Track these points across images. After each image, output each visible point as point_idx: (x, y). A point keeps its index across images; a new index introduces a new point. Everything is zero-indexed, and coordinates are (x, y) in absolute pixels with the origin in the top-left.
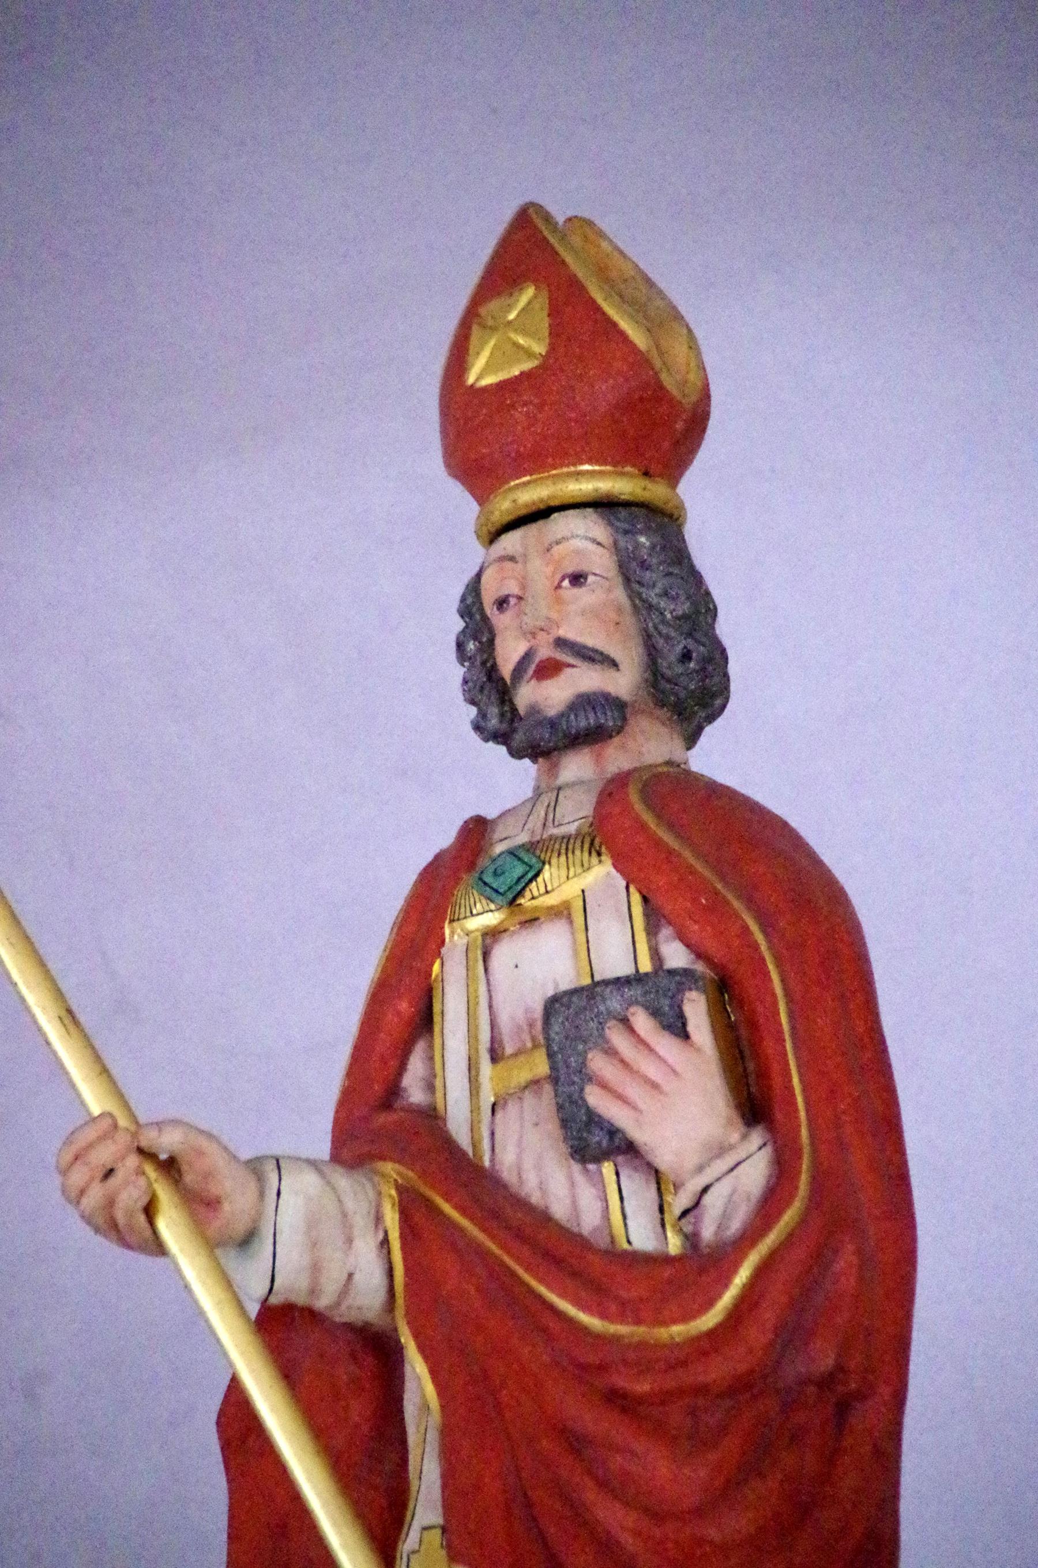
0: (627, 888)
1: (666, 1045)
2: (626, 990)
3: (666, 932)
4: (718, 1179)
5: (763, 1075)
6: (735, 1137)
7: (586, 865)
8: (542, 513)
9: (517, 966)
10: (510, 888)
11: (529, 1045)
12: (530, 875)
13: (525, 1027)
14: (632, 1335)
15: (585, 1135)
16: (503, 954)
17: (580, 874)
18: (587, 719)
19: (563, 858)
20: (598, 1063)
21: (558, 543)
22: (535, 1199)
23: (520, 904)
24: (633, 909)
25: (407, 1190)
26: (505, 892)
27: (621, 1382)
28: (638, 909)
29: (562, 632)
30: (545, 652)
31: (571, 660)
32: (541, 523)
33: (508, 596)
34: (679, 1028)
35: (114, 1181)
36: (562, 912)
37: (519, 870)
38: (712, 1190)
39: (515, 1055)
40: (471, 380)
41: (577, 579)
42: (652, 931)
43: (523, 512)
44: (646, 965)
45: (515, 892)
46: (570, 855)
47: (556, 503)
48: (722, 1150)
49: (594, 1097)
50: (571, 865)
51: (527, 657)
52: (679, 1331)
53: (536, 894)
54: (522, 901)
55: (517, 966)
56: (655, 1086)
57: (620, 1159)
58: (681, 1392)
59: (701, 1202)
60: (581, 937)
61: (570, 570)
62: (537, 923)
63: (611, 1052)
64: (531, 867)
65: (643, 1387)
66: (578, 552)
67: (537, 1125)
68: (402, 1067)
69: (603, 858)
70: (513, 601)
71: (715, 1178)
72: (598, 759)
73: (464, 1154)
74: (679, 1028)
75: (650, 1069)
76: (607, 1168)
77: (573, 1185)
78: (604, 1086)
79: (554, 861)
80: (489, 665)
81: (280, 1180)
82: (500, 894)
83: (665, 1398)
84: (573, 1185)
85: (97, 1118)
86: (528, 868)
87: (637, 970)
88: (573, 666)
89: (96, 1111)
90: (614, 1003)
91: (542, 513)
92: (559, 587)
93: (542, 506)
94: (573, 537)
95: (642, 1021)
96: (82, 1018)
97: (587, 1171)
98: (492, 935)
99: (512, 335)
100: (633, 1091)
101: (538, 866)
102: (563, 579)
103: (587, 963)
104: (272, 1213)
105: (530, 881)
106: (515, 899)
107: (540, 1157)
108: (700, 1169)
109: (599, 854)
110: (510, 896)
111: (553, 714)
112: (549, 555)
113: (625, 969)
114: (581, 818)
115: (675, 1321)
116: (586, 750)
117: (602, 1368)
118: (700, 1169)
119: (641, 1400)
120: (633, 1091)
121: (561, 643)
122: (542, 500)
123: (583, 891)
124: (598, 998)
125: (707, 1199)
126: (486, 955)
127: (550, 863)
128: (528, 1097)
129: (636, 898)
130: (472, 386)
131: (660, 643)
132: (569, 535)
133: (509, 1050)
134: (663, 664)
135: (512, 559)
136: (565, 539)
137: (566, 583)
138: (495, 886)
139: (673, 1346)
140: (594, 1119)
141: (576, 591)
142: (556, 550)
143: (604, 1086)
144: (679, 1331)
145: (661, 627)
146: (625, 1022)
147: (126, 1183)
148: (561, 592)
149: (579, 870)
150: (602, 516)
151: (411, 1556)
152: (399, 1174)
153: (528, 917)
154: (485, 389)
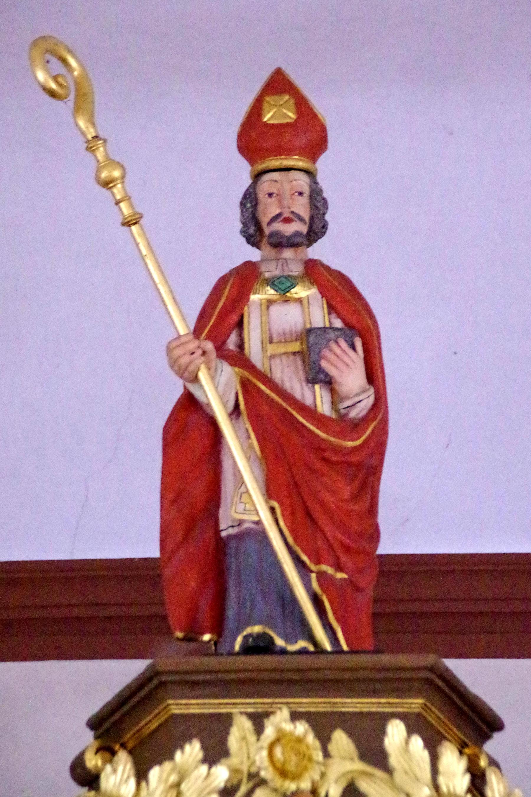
1: (350, 352)
3: (333, 315)
11: (283, 340)
16: (275, 310)
20: (326, 352)
21: (295, 180)
22: (289, 390)
28: (325, 306)
30: (287, 214)
32: (287, 172)
35: (193, 356)
36: (300, 301)
37: (289, 284)
38: (362, 402)
39: (276, 343)
40: (265, 120)
41: (301, 194)
42: (329, 313)
47: (294, 167)
48: (364, 391)
49: (324, 364)
51: (279, 215)
52: (350, 444)
56: (347, 365)
61: (300, 190)
63: (331, 350)
65: (335, 459)
68: (228, 336)
70: (275, 195)
74: (353, 347)
75: (346, 359)
76: (317, 387)
78: (328, 360)
85: (182, 336)
92: (293, 194)
93: (289, 167)
95: (344, 344)
98: (270, 303)
99: (285, 111)
100: (341, 365)
108: (357, 395)
116: (293, 249)
118: (357, 395)
121: (293, 213)
126: (268, 307)
128: (284, 358)
129: (325, 302)
133: (275, 340)
134: (314, 227)
137: (296, 194)
140: (321, 370)
142: (294, 183)
143: (328, 360)
146: (337, 343)
148: (293, 197)
153: (287, 299)
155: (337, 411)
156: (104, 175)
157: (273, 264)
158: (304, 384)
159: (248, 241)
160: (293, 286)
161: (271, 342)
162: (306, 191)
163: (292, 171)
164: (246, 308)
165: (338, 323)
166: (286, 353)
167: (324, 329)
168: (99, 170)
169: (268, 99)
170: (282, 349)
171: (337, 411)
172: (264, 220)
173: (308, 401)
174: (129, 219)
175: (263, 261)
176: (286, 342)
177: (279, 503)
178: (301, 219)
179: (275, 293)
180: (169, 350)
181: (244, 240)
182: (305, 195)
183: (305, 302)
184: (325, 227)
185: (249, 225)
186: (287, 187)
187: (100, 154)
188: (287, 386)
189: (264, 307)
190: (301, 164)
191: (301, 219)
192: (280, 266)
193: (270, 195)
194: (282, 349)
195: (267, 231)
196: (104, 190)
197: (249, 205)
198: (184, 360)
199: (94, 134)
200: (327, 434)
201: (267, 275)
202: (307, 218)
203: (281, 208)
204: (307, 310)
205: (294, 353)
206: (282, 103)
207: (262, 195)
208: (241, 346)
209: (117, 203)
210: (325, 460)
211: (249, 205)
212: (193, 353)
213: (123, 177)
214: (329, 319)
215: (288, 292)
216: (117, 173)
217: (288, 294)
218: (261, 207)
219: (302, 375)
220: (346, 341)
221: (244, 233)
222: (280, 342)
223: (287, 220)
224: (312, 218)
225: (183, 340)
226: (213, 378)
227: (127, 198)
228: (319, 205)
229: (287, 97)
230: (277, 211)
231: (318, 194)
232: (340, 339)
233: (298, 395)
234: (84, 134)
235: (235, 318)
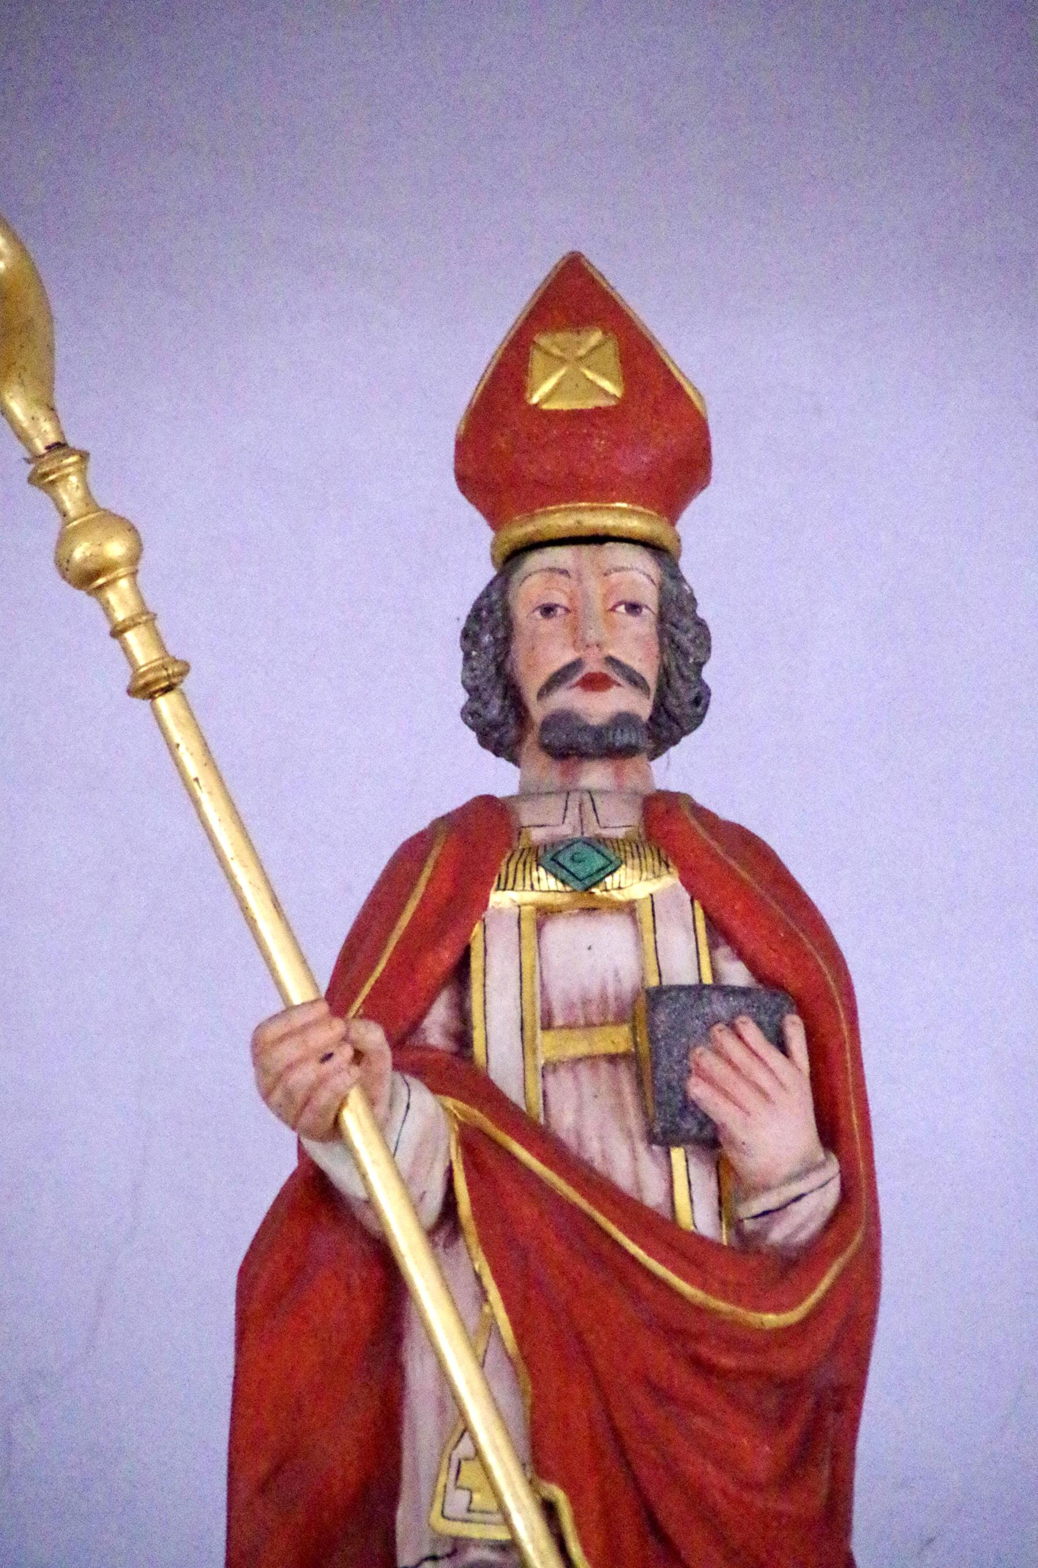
0: (692, 901)
1: (774, 1057)
2: (731, 999)
3: (724, 951)
4: (811, 1191)
5: (834, 1104)
6: (821, 1156)
7: (657, 873)
8: (599, 539)
9: (590, 948)
10: (591, 875)
11: (582, 1022)
12: (609, 869)
13: (579, 1005)
14: (732, 1313)
15: (678, 1119)
16: (557, 932)
17: (651, 879)
18: (631, 736)
19: (637, 861)
21: (617, 570)
23: (593, 893)
24: (698, 924)
25: (465, 1125)
26: (584, 879)
27: (704, 1350)
28: (701, 924)
29: (612, 652)
30: (593, 666)
31: (619, 679)
32: (594, 547)
33: (557, 606)
34: (782, 1046)
35: (328, 1066)
36: (629, 909)
37: (600, 862)
38: (805, 1199)
39: (562, 1027)
41: (634, 608)
42: (713, 946)
43: (583, 533)
44: (708, 979)
45: (594, 881)
46: (642, 859)
49: (698, 1090)
50: (644, 869)
52: (772, 1320)
53: (609, 887)
54: (594, 890)
55: (590, 948)
57: (690, 1147)
58: (757, 1374)
59: (789, 1207)
60: (648, 937)
61: (629, 598)
62: (597, 912)
63: (718, 1052)
64: (611, 862)
65: (727, 1361)
66: (633, 582)
67: (596, 1096)
68: (423, 1015)
69: (671, 870)
71: (809, 1190)
72: (618, 774)
73: (516, 1106)
74: (782, 1046)
76: (677, 1155)
77: (635, 1159)
78: (709, 1080)
79: (630, 862)
80: (499, 659)
81: (409, 1095)
82: (577, 878)
83: (741, 1375)
84: (635, 1159)
86: (608, 863)
87: (701, 980)
88: (619, 685)
89: (297, 999)
90: (720, 1007)
91: (599, 539)
94: (633, 569)
95: (751, 1032)
96: (285, 908)
97: (652, 1150)
98: (545, 914)
100: (743, 1091)
101: (617, 863)
102: (620, 603)
103: (655, 962)
104: (399, 1124)
105: (608, 875)
106: (590, 887)
107: (602, 1127)
109: (668, 866)
110: (587, 882)
111: (595, 724)
112: (605, 578)
113: (689, 979)
114: (629, 826)
115: (768, 1311)
117: (699, 1337)
119: (724, 1374)
120: (743, 1091)
121: (611, 660)
122: (605, 527)
123: (651, 895)
124: (705, 1000)
125: (795, 1207)
126: (539, 927)
127: (626, 864)
128: (584, 1072)
129: (700, 913)
130: (536, 405)
131: (678, 684)
132: (629, 566)
133: (559, 1021)
135: (564, 572)
136: (621, 569)
137: (622, 609)
138: (572, 870)
139: (760, 1331)
140: (689, 1106)
141: (631, 619)
142: (614, 577)
143: (709, 1080)
144: (772, 1320)
145: (684, 669)
146: (732, 1027)
147: (339, 1071)
149: (651, 876)
150: (653, 555)
151: (463, 1463)
152: (455, 1108)
153: (592, 905)
154: (546, 414)
155: (735, 1225)
156: (81, 552)
157: (555, 804)
158: (641, 1147)
159: (484, 740)
160: (610, 868)
161: (547, 1025)
162: (649, 597)
163: (609, 545)
164: (477, 929)
165: (737, 974)
166: (591, 1059)
167: (698, 990)
168: (65, 539)
169: (543, 340)
170: (578, 1046)
171: (735, 1225)
172: (531, 686)
173: (653, 1196)
174: (150, 677)
175: (526, 794)
176: (589, 1025)
177: (565, 1487)
178: (635, 680)
179: (560, 886)
180: (259, 1048)
181: (471, 737)
182: (645, 611)
183: (644, 913)
184: (701, 700)
185: (485, 696)
186: (594, 587)
187: (70, 494)
188: (593, 1151)
189: (528, 927)
190: (635, 525)
191: (635, 680)
192: (573, 813)
193: (548, 610)
194: (578, 1046)
195: (538, 712)
196: (81, 595)
197: (486, 639)
198: (305, 1075)
199: (52, 438)
200: (703, 1286)
201: (538, 835)
202: (651, 677)
203: (577, 649)
204: (648, 937)
205: (612, 1059)
206: (582, 352)
207: (524, 613)
208: (462, 1038)
209: (117, 632)
210: (702, 1367)
211: (486, 639)
212: (329, 1056)
213: (134, 559)
214: (712, 961)
215: (595, 884)
216: (116, 549)
217: (596, 891)
218: (520, 648)
219: (634, 1122)
220: (759, 1024)
221: (471, 715)
222: (570, 1027)
223: (595, 683)
224: (665, 674)
225: (298, 1020)
226: (382, 1127)
227: (145, 617)
228: (684, 639)
229: (596, 337)
230: (569, 657)
231: (681, 610)
232: (743, 1018)
233: (623, 1179)
234: (23, 437)
235: (447, 956)
